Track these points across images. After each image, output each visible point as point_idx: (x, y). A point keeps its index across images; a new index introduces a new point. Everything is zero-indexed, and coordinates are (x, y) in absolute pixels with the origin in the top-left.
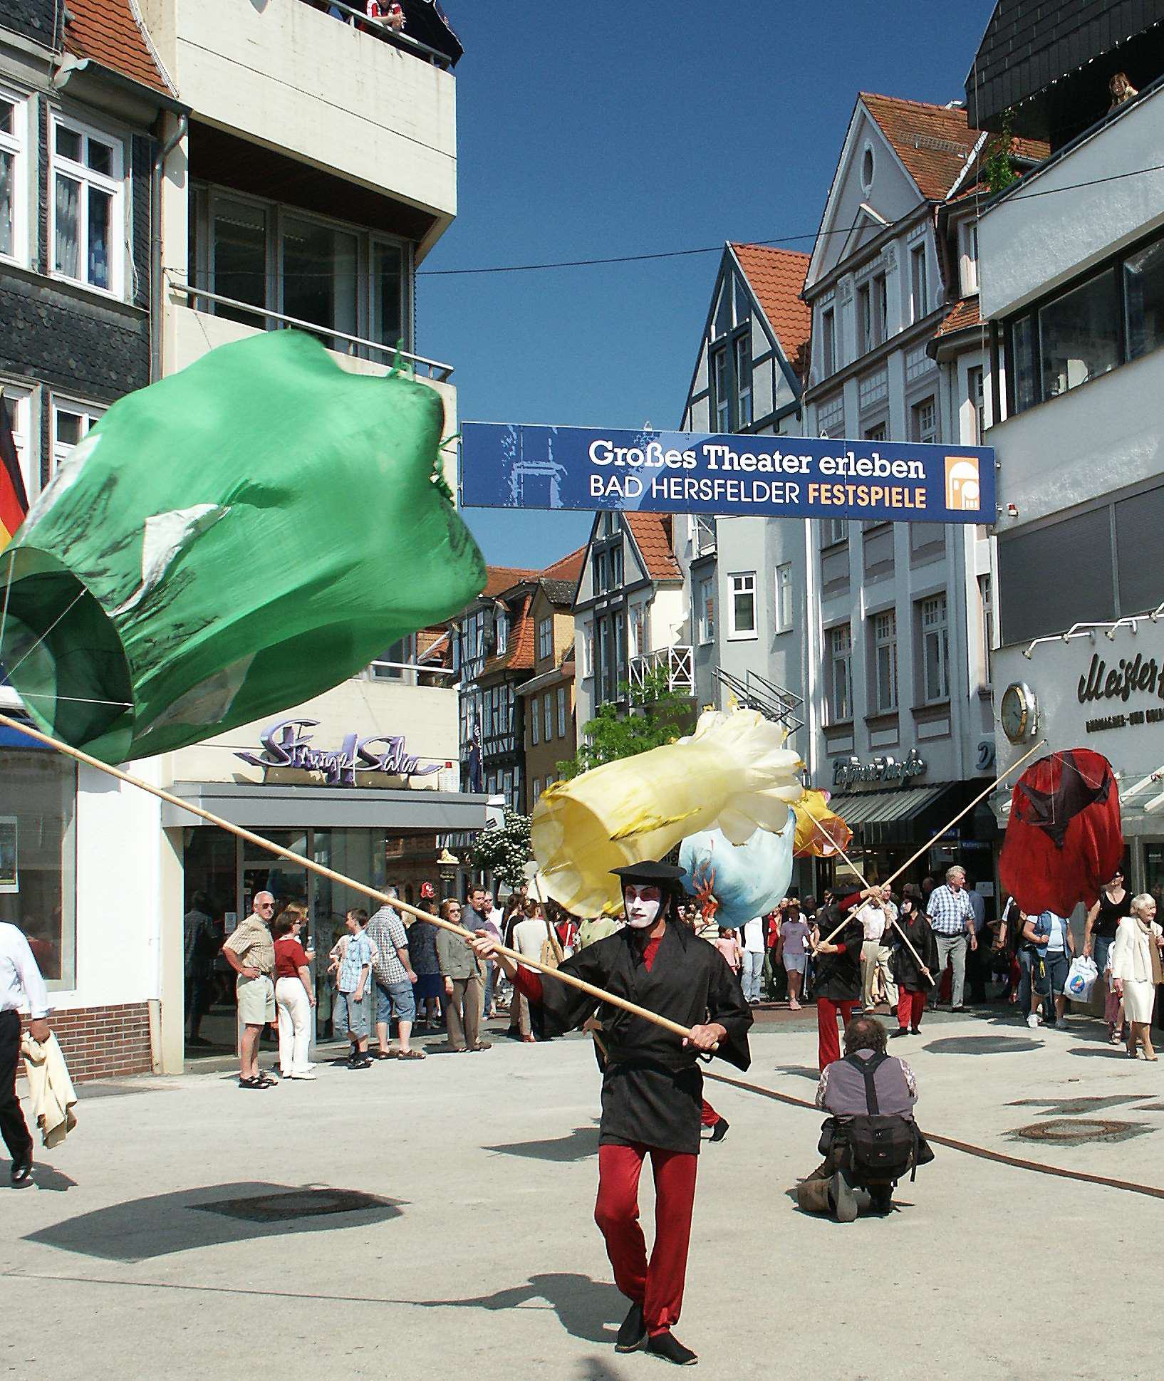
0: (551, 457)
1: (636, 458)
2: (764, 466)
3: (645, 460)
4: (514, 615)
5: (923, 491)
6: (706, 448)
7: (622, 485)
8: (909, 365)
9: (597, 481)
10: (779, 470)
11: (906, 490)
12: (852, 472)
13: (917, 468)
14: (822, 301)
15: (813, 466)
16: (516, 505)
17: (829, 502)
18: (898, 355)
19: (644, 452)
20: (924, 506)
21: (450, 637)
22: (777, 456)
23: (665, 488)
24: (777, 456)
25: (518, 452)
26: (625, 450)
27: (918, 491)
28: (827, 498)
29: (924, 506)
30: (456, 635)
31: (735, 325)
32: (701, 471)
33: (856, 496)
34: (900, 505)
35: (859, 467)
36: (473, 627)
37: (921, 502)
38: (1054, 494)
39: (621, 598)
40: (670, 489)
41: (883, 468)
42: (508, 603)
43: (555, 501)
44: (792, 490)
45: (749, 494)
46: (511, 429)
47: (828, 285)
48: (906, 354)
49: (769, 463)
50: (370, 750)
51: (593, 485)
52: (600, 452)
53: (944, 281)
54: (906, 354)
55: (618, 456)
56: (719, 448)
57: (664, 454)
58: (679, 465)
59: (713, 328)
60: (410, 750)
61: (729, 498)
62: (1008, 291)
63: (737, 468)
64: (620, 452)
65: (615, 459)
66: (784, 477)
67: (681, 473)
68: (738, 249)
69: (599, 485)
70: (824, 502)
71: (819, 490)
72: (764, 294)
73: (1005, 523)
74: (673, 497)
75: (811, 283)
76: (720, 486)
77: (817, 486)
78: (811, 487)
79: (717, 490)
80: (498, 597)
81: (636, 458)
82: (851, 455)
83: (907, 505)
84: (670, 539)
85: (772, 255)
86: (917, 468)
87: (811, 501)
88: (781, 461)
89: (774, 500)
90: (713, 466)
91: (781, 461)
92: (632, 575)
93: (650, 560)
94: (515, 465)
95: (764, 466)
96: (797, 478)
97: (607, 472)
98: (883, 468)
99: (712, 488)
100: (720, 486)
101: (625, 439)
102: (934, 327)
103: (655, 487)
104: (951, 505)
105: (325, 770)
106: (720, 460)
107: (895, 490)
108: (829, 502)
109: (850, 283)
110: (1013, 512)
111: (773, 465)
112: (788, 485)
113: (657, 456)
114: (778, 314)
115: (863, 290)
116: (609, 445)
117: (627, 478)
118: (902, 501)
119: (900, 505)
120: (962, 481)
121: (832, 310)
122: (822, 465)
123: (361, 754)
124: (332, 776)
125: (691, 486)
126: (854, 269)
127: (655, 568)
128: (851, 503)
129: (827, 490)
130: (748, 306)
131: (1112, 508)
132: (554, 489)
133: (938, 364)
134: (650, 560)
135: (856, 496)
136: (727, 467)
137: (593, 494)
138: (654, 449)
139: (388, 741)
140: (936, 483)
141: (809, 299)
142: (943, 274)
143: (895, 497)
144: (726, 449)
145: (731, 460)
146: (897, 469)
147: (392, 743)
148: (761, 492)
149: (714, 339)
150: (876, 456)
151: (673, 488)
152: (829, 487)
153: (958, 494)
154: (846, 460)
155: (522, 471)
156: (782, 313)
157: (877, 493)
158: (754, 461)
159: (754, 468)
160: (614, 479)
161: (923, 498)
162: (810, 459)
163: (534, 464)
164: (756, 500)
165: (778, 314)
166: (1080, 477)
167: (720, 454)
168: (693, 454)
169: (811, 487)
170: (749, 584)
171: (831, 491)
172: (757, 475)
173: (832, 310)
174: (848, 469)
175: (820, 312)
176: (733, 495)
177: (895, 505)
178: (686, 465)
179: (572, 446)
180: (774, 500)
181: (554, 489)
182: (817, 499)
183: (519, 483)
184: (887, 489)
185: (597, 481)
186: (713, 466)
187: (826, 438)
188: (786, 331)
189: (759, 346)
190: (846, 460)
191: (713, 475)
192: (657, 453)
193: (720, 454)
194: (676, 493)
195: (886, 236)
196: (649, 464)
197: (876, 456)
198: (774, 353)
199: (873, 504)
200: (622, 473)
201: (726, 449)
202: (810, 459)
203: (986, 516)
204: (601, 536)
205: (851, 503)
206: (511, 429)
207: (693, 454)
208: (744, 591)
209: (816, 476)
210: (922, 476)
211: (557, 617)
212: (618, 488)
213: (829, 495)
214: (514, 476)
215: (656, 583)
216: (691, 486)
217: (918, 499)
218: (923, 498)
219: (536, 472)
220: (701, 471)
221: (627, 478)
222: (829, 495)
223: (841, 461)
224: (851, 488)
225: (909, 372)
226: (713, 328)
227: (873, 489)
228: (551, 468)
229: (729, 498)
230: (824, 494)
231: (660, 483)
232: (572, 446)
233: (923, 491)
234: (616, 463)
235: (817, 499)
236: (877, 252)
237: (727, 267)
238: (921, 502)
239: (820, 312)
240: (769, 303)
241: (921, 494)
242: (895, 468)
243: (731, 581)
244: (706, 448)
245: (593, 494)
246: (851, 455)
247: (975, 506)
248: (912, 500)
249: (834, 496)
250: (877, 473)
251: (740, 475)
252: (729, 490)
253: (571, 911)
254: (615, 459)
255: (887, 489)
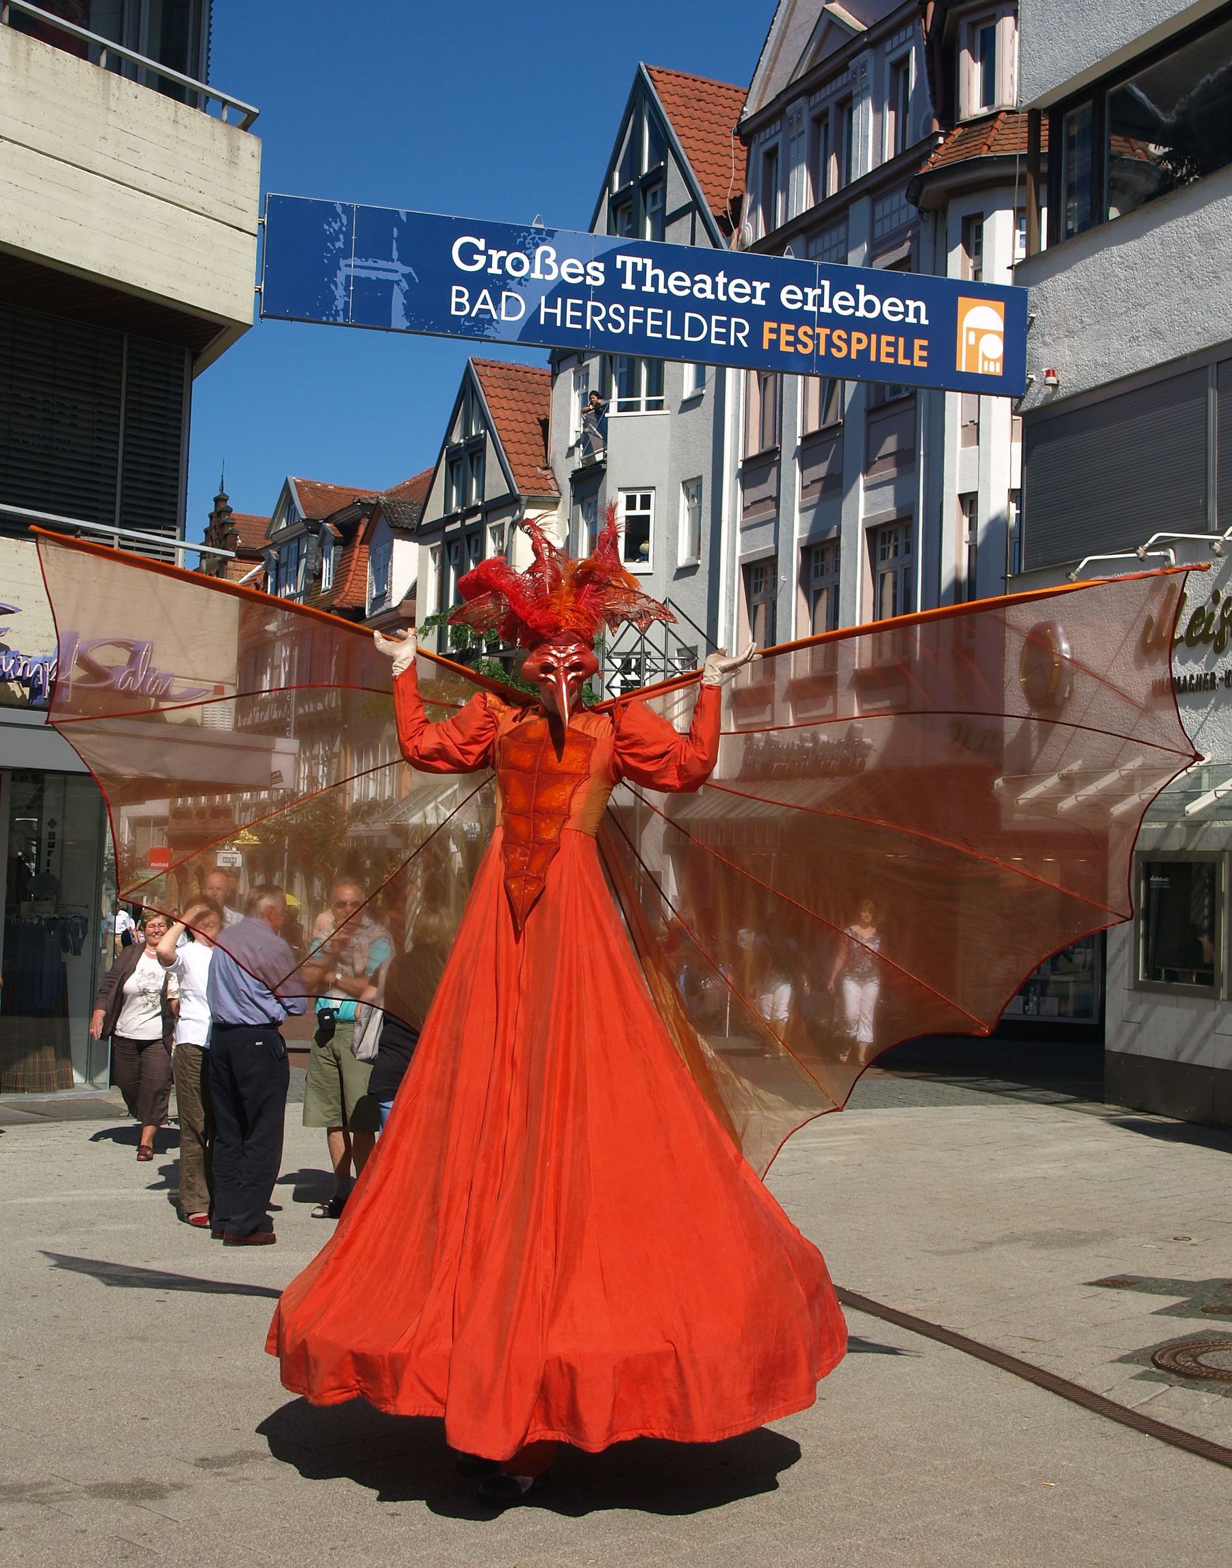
0: (395, 255)
1: (518, 265)
2: (702, 291)
3: (532, 270)
4: (347, 536)
5: (925, 343)
6: (620, 259)
7: (497, 303)
8: (878, 217)
9: (460, 294)
10: (723, 298)
11: (901, 340)
12: (826, 309)
13: (917, 310)
14: (762, 136)
15: (772, 296)
16: (340, 320)
17: (791, 349)
18: (865, 202)
19: (531, 259)
20: (924, 364)
21: (265, 567)
22: (721, 279)
23: (558, 311)
24: (721, 279)
25: (348, 241)
26: (504, 253)
27: (918, 343)
28: (788, 343)
29: (924, 364)
30: (273, 565)
31: (645, 170)
32: (611, 292)
33: (830, 343)
34: (891, 361)
35: (836, 302)
36: (294, 556)
37: (921, 359)
38: (1120, 352)
39: (479, 517)
40: (565, 313)
41: (870, 306)
42: (340, 527)
43: (398, 319)
44: (740, 328)
45: (677, 329)
46: (339, 209)
47: (773, 114)
48: (874, 202)
49: (708, 287)
50: (100, 657)
51: (454, 300)
52: (468, 253)
53: (934, 103)
54: (874, 202)
55: (495, 260)
56: (639, 261)
57: (559, 262)
58: (580, 279)
59: (616, 176)
60: (162, 663)
61: (649, 334)
62: (1063, 63)
63: (662, 290)
64: (496, 255)
65: (489, 263)
66: (729, 308)
67: (582, 291)
68: (654, 74)
69: (464, 300)
70: (783, 348)
71: (776, 331)
72: (686, 131)
73: (1035, 397)
74: (568, 325)
75: (749, 110)
76: (637, 315)
77: (774, 325)
78: (767, 325)
79: (632, 320)
80: (326, 521)
81: (518, 265)
82: (826, 283)
83: (902, 361)
84: (546, 445)
85: (698, 84)
86: (917, 310)
87: (766, 346)
88: (726, 286)
89: (713, 341)
90: (628, 285)
91: (726, 286)
92: (496, 485)
93: (520, 470)
94: (342, 263)
95: (702, 291)
96: (747, 311)
97: (477, 282)
98: (870, 306)
99: (625, 317)
100: (637, 315)
101: (506, 237)
102: (918, 163)
103: (543, 310)
104: (963, 366)
105: (24, 681)
106: (639, 278)
107: (884, 339)
108: (791, 349)
109: (803, 109)
110: (1052, 380)
111: (715, 291)
112: (734, 320)
113: (549, 264)
114: (702, 157)
115: (819, 120)
116: (481, 244)
117: (504, 294)
118: (894, 355)
119: (891, 361)
120: (980, 333)
121: (775, 149)
122: (784, 296)
123: (84, 662)
124: (37, 691)
125: (596, 312)
126: (809, 92)
127: (525, 481)
128: (822, 353)
129: (788, 332)
130: (662, 144)
131: (1212, 371)
132: (398, 300)
133: (920, 212)
134: (520, 470)
135: (830, 343)
136: (648, 288)
137: (453, 312)
138: (546, 255)
139: (126, 645)
140: (943, 332)
141: (746, 133)
142: (933, 94)
143: (885, 349)
144: (649, 262)
145: (655, 279)
146: (888, 308)
147: (134, 651)
148: (696, 328)
149: (616, 189)
150: (861, 288)
151: (569, 313)
152: (792, 327)
153: (973, 350)
154: (818, 291)
155: (353, 272)
156: (707, 156)
157: (859, 341)
158: (688, 283)
159: (687, 292)
160: (485, 292)
161: (925, 354)
162: (767, 285)
163: (370, 263)
164: (687, 338)
165: (702, 157)
166: (1163, 326)
167: (640, 268)
168: (601, 266)
169: (767, 325)
170: (646, 503)
171: (794, 333)
172: (691, 303)
173: (775, 149)
174: (821, 304)
175: (760, 150)
176: (655, 329)
177: (884, 359)
178: (589, 281)
179: (427, 239)
180: (713, 341)
181: (398, 300)
182: (775, 343)
183: (346, 288)
184: (874, 337)
185: (460, 294)
186: (628, 285)
187: (792, 257)
188: (712, 178)
189: (677, 196)
190: (818, 291)
191: (628, 299)
192: (549, 261)
193: (640, 268)
194: (574, 320)
195: (857, 46)
196: (537, 275)
197: (861, 288)
198: (695, 206)
199: (854, 356)
200: (498, 284)
201: (649, 262)
202: (767, 285)
203: (1011, 382)
204: (457, 438)
205: (822, 353)
206: (339, 209)
207: (601, 266)
208: (638, 512)
209: (774, 310)
210: (924, 321)
211: (398, 543)
212: (491, 307)
213: (791, 338)
214: (340, 278)
215: (524, 499)
216: (596, 312)
217: (918, 353)
218: (925, 354)
219: (373, 275)
220: (611, 292)
221: (504, 294)
222: (791, 338)
223: (812, 293)
224: (823, 332)
225: (878, 227)
226: (616, 176)
227: (855, 335)
228: (395, 270)
229: (649, 334)
230: (784, 338)
231: (551, 303)
232: (427, 239)
233: (925, 343)
234: (490, 271)
235: (775, 343)
236: (844, 68)
237: (640, 96)
238: (921, 359)
239: (760, 150)
240: (691, 142)
241: (922, 348)
242: (886, 308)
243: (622, 498)
244: (620, 259)
245: (453, 312)
246: (826, 283)
247: (996, 369)
248: (909, 354)
249: (798, 340)
250: (861, 312)
251: (667, 301)
252: (650, 322)
253: (594, 753)
254: (489, 263)
255: (874, 337)
